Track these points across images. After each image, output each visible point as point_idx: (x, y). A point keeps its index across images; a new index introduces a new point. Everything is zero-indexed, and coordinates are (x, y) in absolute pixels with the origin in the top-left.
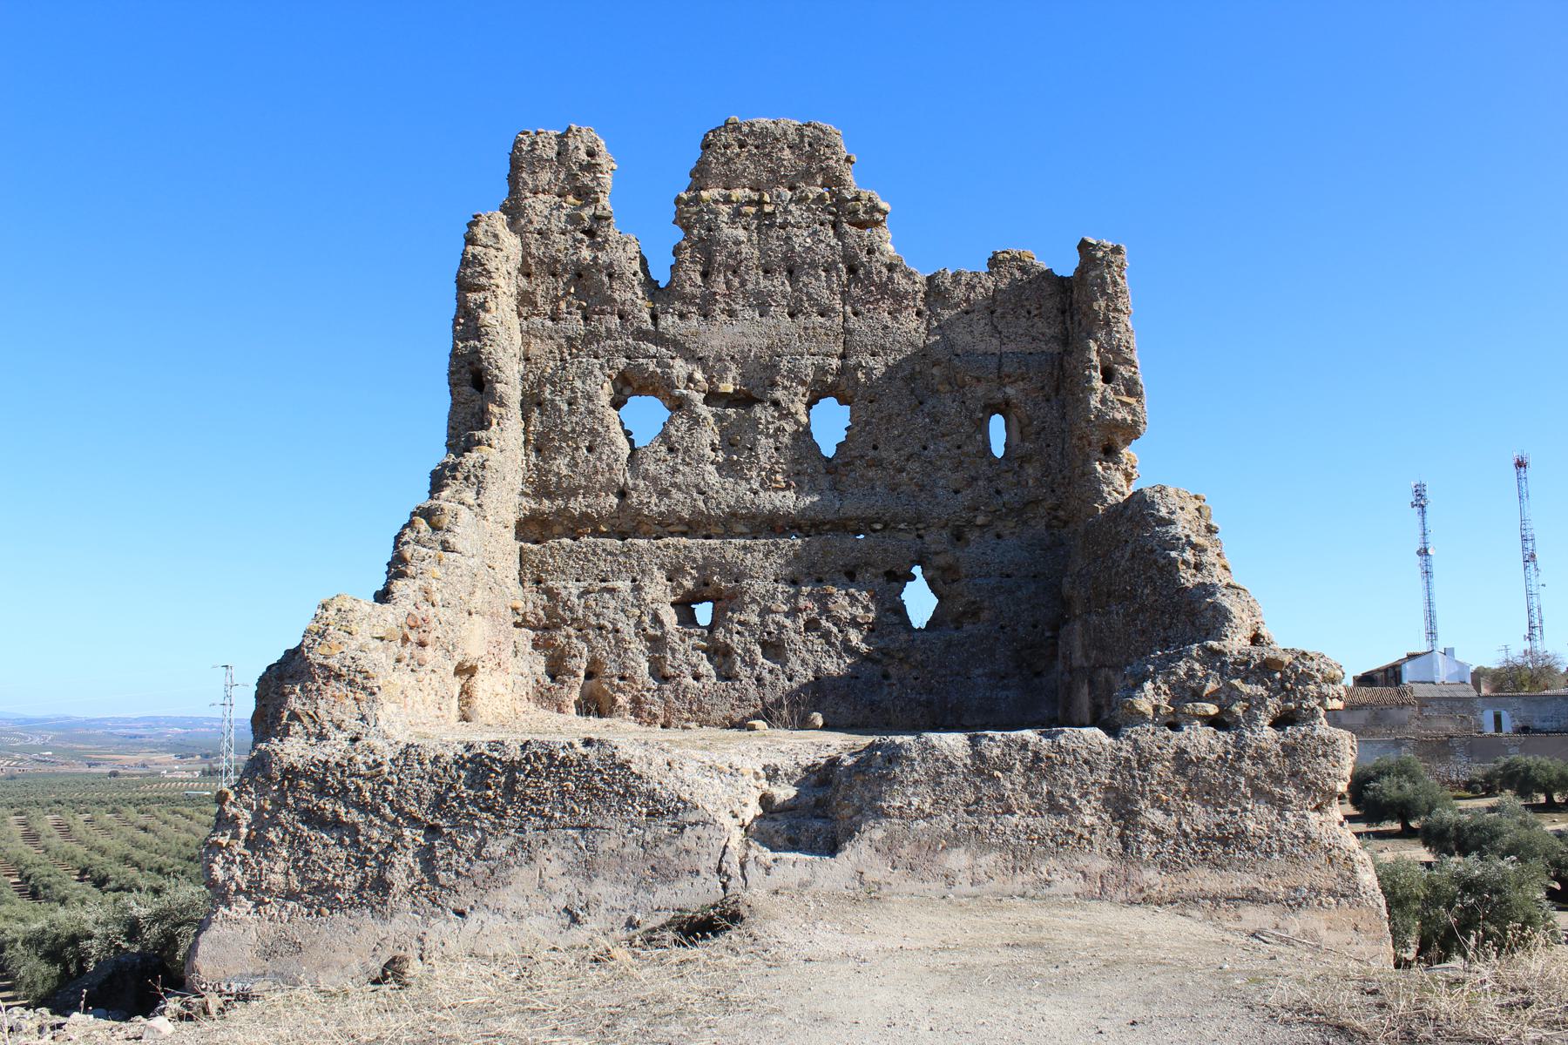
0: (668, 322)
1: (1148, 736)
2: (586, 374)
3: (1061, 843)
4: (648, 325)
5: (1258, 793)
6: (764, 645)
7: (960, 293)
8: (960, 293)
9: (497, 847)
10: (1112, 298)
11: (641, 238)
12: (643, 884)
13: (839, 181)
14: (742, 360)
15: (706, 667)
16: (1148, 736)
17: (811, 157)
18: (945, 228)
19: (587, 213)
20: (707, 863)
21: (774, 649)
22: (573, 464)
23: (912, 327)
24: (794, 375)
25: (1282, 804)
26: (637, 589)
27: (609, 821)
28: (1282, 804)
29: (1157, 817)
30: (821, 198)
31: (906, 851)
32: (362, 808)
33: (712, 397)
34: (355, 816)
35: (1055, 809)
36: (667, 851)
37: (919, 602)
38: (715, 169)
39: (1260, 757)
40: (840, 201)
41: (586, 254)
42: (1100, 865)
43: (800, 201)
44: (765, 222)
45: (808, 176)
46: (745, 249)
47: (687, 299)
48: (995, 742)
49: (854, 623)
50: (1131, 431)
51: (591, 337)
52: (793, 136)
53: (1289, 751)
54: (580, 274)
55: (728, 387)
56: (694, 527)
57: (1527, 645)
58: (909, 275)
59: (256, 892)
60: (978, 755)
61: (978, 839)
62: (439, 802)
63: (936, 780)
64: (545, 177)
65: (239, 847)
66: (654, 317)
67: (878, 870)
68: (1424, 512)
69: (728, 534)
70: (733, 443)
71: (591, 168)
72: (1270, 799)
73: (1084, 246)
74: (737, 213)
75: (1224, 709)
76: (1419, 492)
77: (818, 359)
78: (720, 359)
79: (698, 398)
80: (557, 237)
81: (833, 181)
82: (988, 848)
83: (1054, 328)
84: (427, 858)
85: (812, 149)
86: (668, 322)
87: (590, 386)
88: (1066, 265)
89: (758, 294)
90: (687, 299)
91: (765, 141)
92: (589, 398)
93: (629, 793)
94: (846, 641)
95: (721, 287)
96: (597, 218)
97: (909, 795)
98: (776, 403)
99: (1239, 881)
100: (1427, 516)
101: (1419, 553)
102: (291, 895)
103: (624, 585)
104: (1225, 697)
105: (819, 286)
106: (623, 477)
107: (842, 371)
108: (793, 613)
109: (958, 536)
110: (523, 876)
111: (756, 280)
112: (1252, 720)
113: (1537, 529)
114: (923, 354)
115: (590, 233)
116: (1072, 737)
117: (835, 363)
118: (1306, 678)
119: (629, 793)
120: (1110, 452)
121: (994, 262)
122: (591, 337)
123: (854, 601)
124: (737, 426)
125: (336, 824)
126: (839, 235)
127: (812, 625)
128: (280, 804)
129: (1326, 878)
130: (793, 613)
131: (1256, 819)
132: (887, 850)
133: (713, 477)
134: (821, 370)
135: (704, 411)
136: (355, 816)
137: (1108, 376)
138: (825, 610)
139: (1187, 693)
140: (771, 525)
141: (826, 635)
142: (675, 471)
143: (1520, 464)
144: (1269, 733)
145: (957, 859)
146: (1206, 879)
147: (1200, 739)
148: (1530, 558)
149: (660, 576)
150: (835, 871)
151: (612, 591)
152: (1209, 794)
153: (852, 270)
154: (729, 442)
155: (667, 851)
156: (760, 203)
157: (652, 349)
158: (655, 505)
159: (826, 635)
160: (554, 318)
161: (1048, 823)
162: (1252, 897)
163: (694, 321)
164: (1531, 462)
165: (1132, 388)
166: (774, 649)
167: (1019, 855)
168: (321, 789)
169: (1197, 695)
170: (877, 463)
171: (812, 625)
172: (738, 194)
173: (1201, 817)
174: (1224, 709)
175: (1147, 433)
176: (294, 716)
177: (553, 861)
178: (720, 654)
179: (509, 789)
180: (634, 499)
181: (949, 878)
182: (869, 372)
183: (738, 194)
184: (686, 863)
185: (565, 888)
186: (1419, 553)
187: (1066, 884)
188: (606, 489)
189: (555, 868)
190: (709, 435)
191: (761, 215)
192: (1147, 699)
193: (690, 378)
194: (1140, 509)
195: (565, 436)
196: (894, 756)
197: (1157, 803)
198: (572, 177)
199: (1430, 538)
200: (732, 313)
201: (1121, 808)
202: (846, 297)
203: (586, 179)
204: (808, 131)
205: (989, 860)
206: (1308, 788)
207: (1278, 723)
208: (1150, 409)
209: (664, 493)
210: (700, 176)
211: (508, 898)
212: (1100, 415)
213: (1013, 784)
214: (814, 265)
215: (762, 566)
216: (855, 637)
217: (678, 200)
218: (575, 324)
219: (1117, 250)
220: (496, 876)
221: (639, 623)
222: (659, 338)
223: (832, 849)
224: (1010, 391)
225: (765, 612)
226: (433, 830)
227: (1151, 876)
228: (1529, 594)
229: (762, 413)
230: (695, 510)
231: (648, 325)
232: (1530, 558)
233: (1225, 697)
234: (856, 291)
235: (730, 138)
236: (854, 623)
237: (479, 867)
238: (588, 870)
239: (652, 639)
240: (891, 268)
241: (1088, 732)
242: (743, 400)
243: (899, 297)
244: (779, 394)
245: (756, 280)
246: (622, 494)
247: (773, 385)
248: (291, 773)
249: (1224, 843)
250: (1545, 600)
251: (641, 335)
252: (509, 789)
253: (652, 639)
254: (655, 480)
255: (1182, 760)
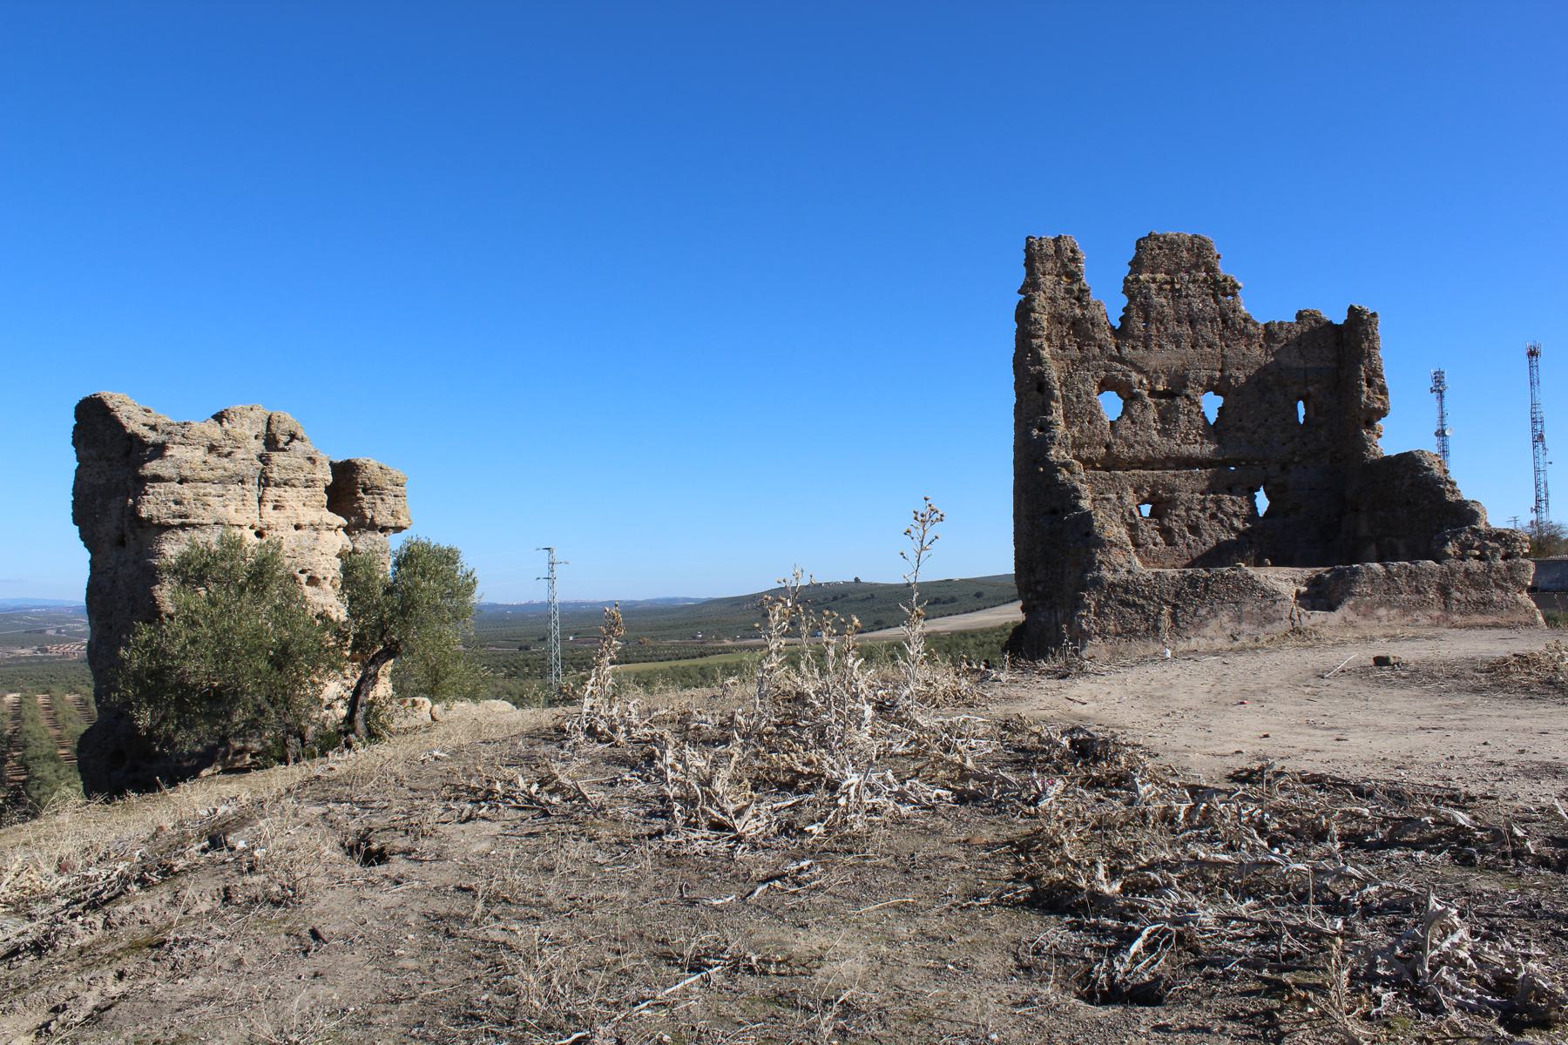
0: (1126, 351)
1: (1453, 563)
2: (1084, 381)
3: (1422, 605)
4: (1115, 353)
5: (1498, 586)
6: (1189, 527)
7: (1283, 335)
8: (1283, 335)
9: (1203, 612)
10: (1372, 342)
11: (1109, 303)
12: (1261, 625)
13: (1214, 270)
14: (1168, 373)
15: (1159, 539)
16: (1453, 563)
17: (1198, 256)
18: (1270, 298)
19: (1075, 287)
20: (1285, 615)
21: (1195, 529)
22: (1081, 431)
23: (1258, 354)
24: (1197, 381)
25: (1506, 590)
26: (1120, 498)
27: (1247, 599)
28: (1506, 590)
29: (1458, 595)
30: (1205, 280)
31: (1362, 609)
32: (1145, 598)
33: (1153, 393)
34: (1142, 601)
35: (1419, 592)
36: (1270, 611)
37: (1262, 502)
38: (1147, 262)
39: (1498, 571)
40: (1216, 282)
41: (1078, 311)
42: (1437, 613)
43: (1194, 282)
44: (1176, 294)
45: (1196, 267)
46: (1166, 310)
47: (1136, 338)
48: (1394, 566)
49: (1235, 515)
50: (1382, 413)
51: (1084, 360)
52: (1188, 243)
53: (1510, 569)
54: (1075, 324)
55: (1160, 387)
56: (1148, 464)
57: (1533, 517)
58: (1255, 324)
59: (1103, 634)
60: (1388, 571)
61: (1389, 604)
62: (1177, 595)
63: (1372, 581)
64: (1049, 265)
65: (1091, 616)
66: (1118, 348)
67: (1352, 617)
68: (1442, 397)
69: (1164, 467)
70: (1167, 419)
71: (1074, 260)
72: (1501, 587)
73: (1351, 309)
74: (1160, 289)
75: (1483, 553)
76: (1438, 378)
77: (1209, 372)
78: (1155, 372)
79: (1146, 393)
80: (1060, 302)
81: (1211, 269)
82: (1393, 607)
83: (1337, 356)
84: (1174, 617)
85: (1200, 252)
86: (1126, 351)
87: (1088, 388)
88: (1339, 317)
89: (1175, 336)
90: (1136, 338)
91: (1172, 245)
92: (1088, 394)
93: (1254, 588)
94: (1232, 524)
95: (1154, 332)
96: (1080, 290)
97: (1363, 588)
98: (1188, 397)
99: (1491, 619)
100: (1446, 400)
101: (1437, 434)
102: (1118, 634)
103: (1113, 496)
104: (1483, 548)
105: (1208, 332)
106: (1109, 437)
107: (1222, 378)
108: (1203, 510)
109: (1283, 468)
110: (1213, 623)
111: (1173, 327)
112: (1494, 557)
113: (1546, 412)
114: (1264, 370)
115: (1078, 299)
116: (1422, 563)
117: (1218, 374)
118: (1515, 540)
119: (1254, 588)
120: (1370, 424)
121: (1300, 316)
122: (1084, 360)
123: (1234, 503)
124: (1168, 409)
125: (1135, 605)
126: (1217, 302)
127: (1213, 516)
128: (1108, 597)
129: (1523, 618)
130: (1203, 510)
131: (1497, 595)
132: (1355, 608)
133: (1156, 437)
134: (1211, 378)
135: (1148, 400)
136: (1142, 601)
137: (1370, 383)
138: (1219, 508)
139: (1465, 547)
140: (1188, 463)
141: (1221, 521)
142: (1136, 434)
143: (1532, 353)
144: (1501, 562)
145: (1382, 612)
146: (1478, 619)
147: (1474, 565)
148: (1539, 438)
149: (1131, 490)
150: (1334, 617)
151: (1108, 499)
152: (1477, 585)
153: (1224, 321)
154: (1163, 418)
155: (1270, 611)
156: (1172, 283)
157: (1119, 366)
158: (1126, 453)
159: (1221, 521)
160: (1062, 348)
161: (1415, 597)
162: (1496, 626)
163: (1141, 351)
164: (1543, 351)
165: (1383, 390)
166: (1195, 529)
167: (1406, 610)
168: (1126, 591)
169: (1471, 547)
170: (1241, 429)
171: (1213, 516)
172: (1159, 276)
173: (1475, 595)
174: (1483, 553)
175: (1391, 414)
176: (1101, 562)
177: (1225, 617)
178: (1166, 532)
179: (1206, 588)
180: (1115, 450)
181: (1379, 619)
182: (1237, 379)
183: (1159, 276)
184: (1277, 615)
185: (1230, 627)
186: (1437, 434)
187: (1424, 621)
188: (1100, 444)
189: (1226, 619)
190: (1152, 414)
191: (1173, 290)
192: (1450, 549)
193: (1141, 382)
194: (1409, 463)
195: (1076, 416)
196: (1355, 572)
197: (1458, 589)
198: (1064, 266)
199: (1447, 421)
200: (1161, 346)
201: (1444, 591)
202: (1222, 337)
203: (1072, 267)
204: (1196, 241)
205: (1393, 612)
206: (1516, 583)
207: (1504, 558)
208: (1393, 400)
209: (1131, 446)
210: (1136, 265)
211: (1208, 632)
212: (1367, 405)
213: (1402, 582)
214: (1204, 319)
215: (1188, 487)
216: (1237, 523)
217: (1126, 280)
218: (1075, 353)
219: (1374, 315)
220: (1203, 623)
221: (1123, 516)
222: (1122, 360)
223: (1331, 608)
224: (1311, 389)
225: (1188, 509)
226: (1175, 606)
227: (1456, 617)
228: (1537, 471)
229: (1181, 402)
230: (1148, 456)
231: (1115, 353)
232: (1539, 438)
233: (1483, 548)
234: (1227, 334)
235: (1153, 244)
236: (1235, 515)
237: (1196, 620)
238: (1239, 619)
239: (1129, 524)
240: (1246, 320)
241: (1430, 562)
242: (1169, 395)
243: (1250, 337)
244: (1189, 391)
245: (1173, 327)
246: (1108, 447)
247: (1186, 386)
248: (1112, 585)
249: (1484, 605)
250: (1552, 476)
251: (1112, 358)
252: (1206, 588)
253: (1129, 524)
254: (1126, 439)
255: (1467, 573)
